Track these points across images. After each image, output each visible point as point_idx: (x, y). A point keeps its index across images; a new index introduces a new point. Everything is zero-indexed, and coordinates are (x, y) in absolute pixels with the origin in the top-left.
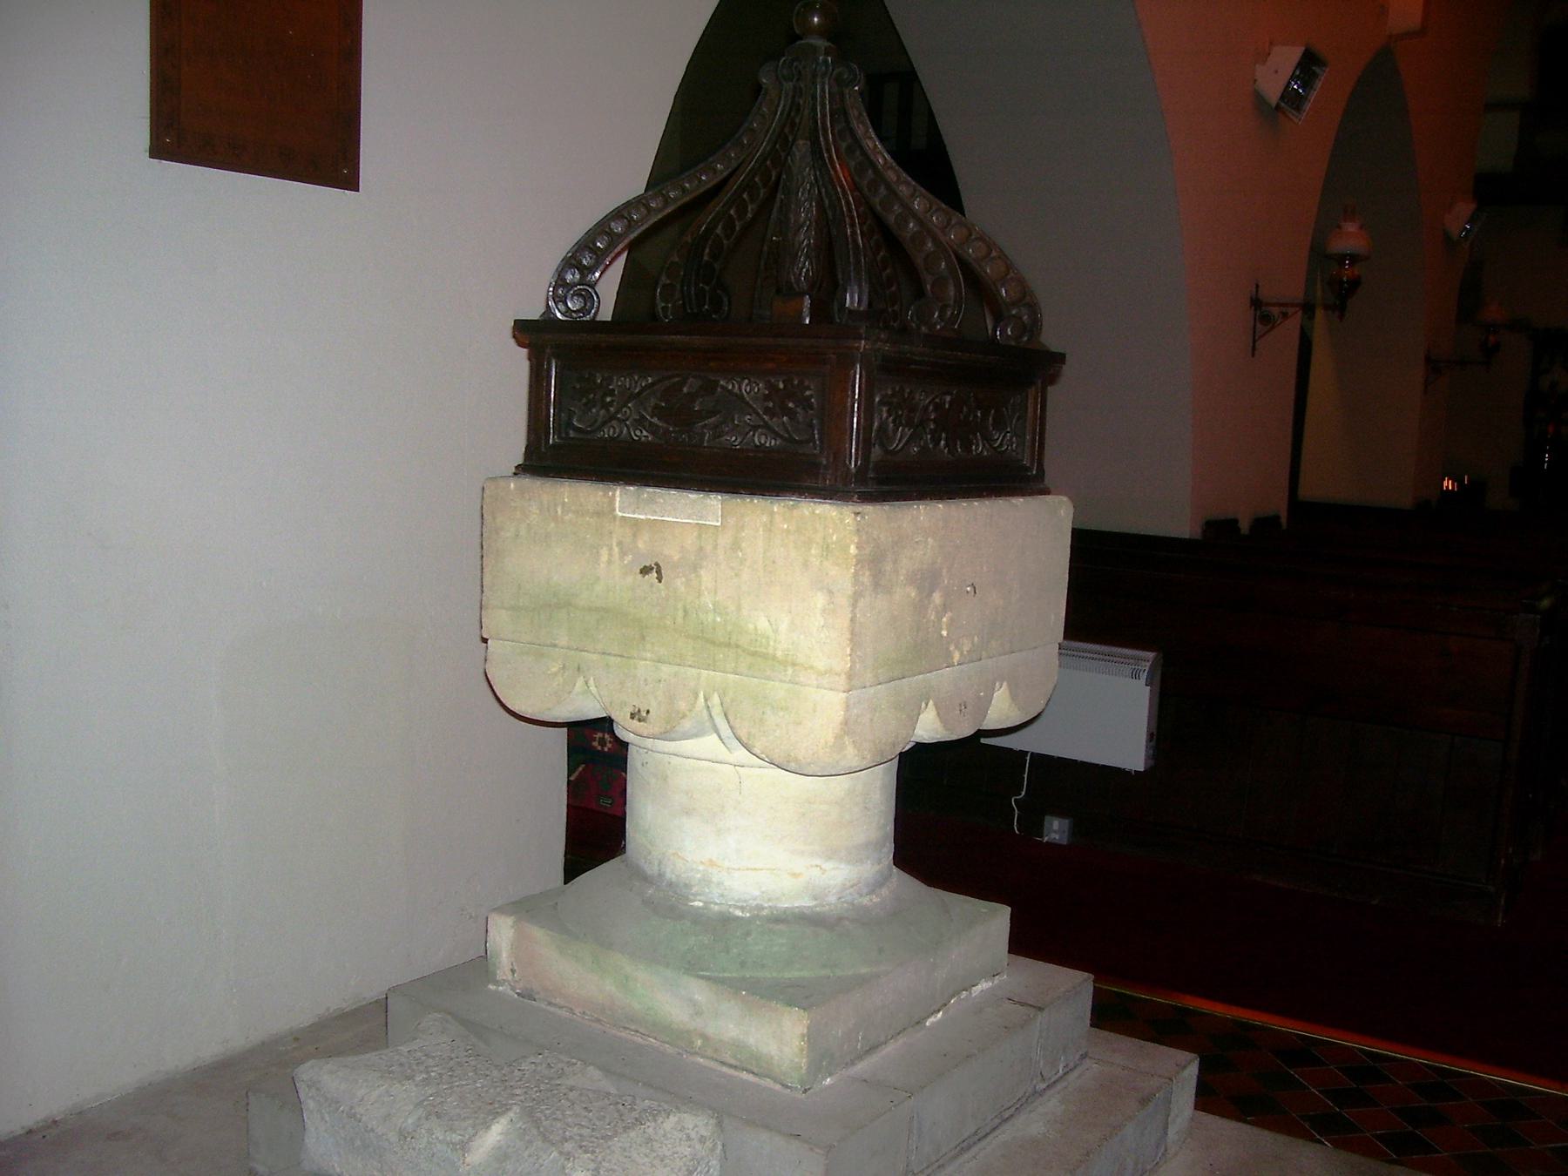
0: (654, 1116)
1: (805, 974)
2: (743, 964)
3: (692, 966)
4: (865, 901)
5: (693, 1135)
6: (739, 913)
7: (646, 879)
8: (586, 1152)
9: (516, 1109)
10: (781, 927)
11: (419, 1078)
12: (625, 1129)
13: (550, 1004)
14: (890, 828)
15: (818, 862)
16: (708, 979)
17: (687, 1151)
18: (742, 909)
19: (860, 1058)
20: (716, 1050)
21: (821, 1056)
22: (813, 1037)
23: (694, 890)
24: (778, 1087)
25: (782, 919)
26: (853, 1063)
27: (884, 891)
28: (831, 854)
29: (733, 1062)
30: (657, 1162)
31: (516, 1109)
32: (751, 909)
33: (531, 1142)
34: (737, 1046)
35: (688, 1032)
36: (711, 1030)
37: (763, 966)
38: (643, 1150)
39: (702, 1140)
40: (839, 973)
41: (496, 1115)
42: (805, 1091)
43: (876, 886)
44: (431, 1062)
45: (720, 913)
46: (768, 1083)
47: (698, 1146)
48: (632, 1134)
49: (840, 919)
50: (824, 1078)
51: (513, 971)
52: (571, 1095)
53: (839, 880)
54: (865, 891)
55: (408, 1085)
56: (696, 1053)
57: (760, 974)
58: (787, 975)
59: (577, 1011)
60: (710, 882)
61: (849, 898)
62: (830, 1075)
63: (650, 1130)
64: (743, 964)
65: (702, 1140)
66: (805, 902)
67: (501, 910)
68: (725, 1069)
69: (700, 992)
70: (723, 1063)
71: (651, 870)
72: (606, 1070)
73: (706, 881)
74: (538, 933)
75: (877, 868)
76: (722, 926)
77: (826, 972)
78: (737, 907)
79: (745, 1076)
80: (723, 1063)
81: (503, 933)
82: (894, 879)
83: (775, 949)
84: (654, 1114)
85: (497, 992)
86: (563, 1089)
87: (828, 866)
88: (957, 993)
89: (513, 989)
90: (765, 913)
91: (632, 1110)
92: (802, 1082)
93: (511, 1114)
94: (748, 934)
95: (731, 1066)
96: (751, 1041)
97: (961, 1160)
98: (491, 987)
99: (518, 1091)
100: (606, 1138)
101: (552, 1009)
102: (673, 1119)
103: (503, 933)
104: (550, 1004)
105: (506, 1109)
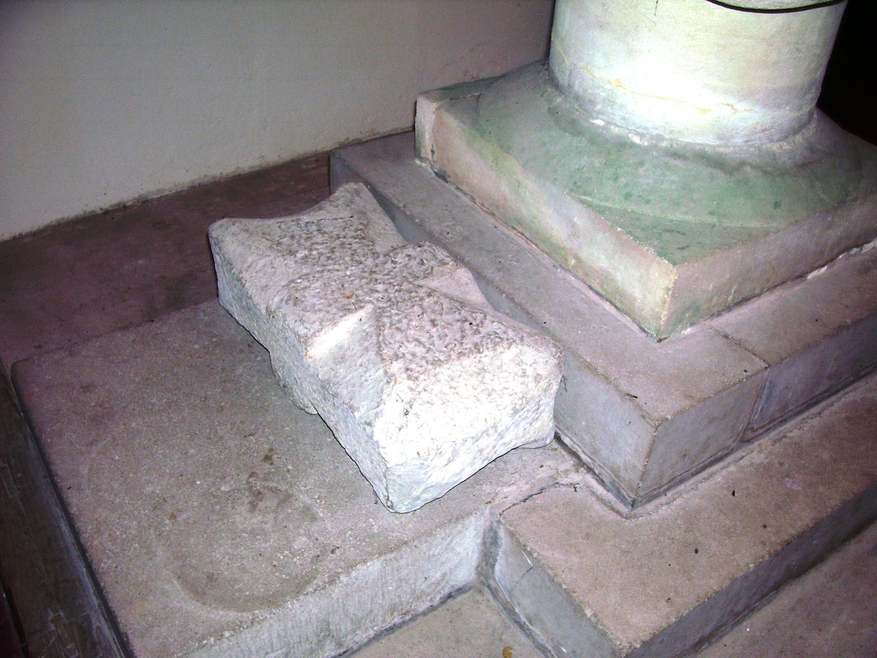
0: (496, 344)
1: (689, 218)
2: (628, 196)
3: (577, 188)
4: (775, 147)
5: (530, 371)
6: (636, 140)
7: (557, 87)
8: (409, 378)
9: (369, 307)
10: (678, 163)
11: (299, 255)
12: (461, 354)
13: (458, 188)
14: (820, 73)
15: (732, 101)
16: (589, 205)
17: (519, 389)
18: (642, 136)
19: (729, 309)
20: (586, 274)
21: (687, 310)
22: (675, 292)
23: (598, 107)
24: (635, 328)
25: (678, 154)
26: (719, 314)
27: (799, 138)
28: (747, 95)
29: (600, 291)
30: (483, 397)
31: (369, 307)
32: (652, 137)
33: (367, 350)
34: (606, 278)
35: (564, 249)
36: (584, 254)
37: (648, 202)
38: (474, 381)
39: (537, 378)
40: (726, 222)
41: (346, 311)
42: (660, 341)
43: (799, 127)
44: (320, 238)
45: (619, 136)
46: (626, 320)
47: (532, 385)
48: (466, 362)
49: (743, 164)
50: (683, 328)
51: (433, 152)
52: (427, 302)
53: (751, 123)
54: (775, 138)
55: (290, 261)
56: (567, 270)
57: (646, 210)
58: (670, 217)
59: (477, 201)
60: (614, 103)
61: (757, 143)
62: (692, 325)
63: (486, 360)
64: (628, 196)
65: (537, 378)
66: (707, 140)
67: (426, 94)
68: (591, 294)
69: (581, 218)
70: (591, 288)
71: (563, 79)
72: (478, 276)
73: (610, 101)
74: (452, 122)
75: (795, 114)
76: (619, 149)
77: (714, 220)
78: (637, 134)
79: (607, 306)
80: (591, 288)
81: (428, 114)
82: (813, 126)
83: (665, 186)
84: (496, 340)
85: (420, 167)
86: (422, 292)
87: (741, 106)
88: (848, 249)
89: (432, 167)
90: (664, 144)
91: (477, 332)
92: (658, 331)
93: (361, 313)
94: (641, 164)
95: (597, 293)
96: (619, 277)
97: (805, 415)
98: (418, 162)
99: (380, 287)
100: (437, 363)
101: (459, 193)
102: (514, 350)
103: (428, 114)
104: (458, 188)
105: (359, 305)
